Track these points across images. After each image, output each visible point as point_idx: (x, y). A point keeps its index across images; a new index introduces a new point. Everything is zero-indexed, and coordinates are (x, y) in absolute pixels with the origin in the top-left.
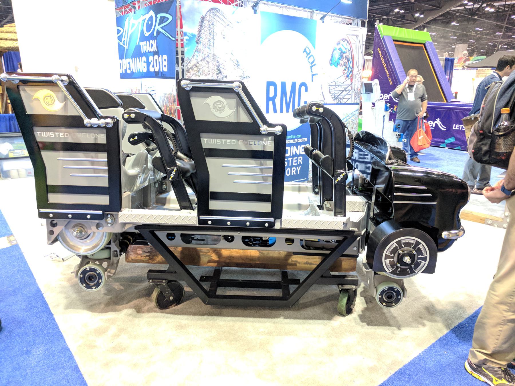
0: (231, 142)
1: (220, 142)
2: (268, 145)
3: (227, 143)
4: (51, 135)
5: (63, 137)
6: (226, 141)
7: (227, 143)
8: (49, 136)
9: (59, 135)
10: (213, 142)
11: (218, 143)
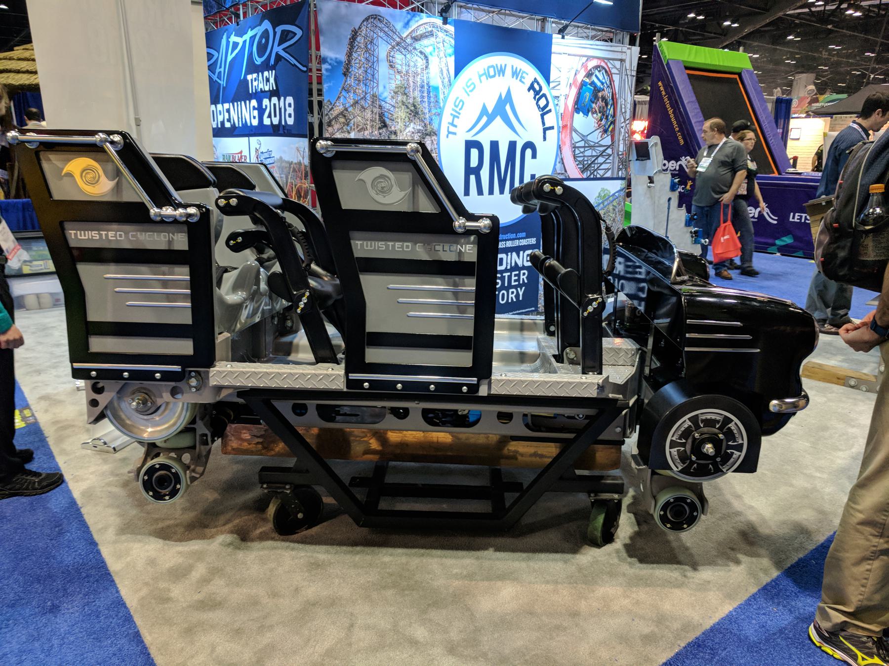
0: (402, 247)
1: (384, 246)
3: (397, 249)
4: (93, 235)
5: (401, 249)
6: (395, 245)
7: (397, 249)
8: (377, 248)
9: (107, 235)
10: (371, 247)
11: (380, 249)
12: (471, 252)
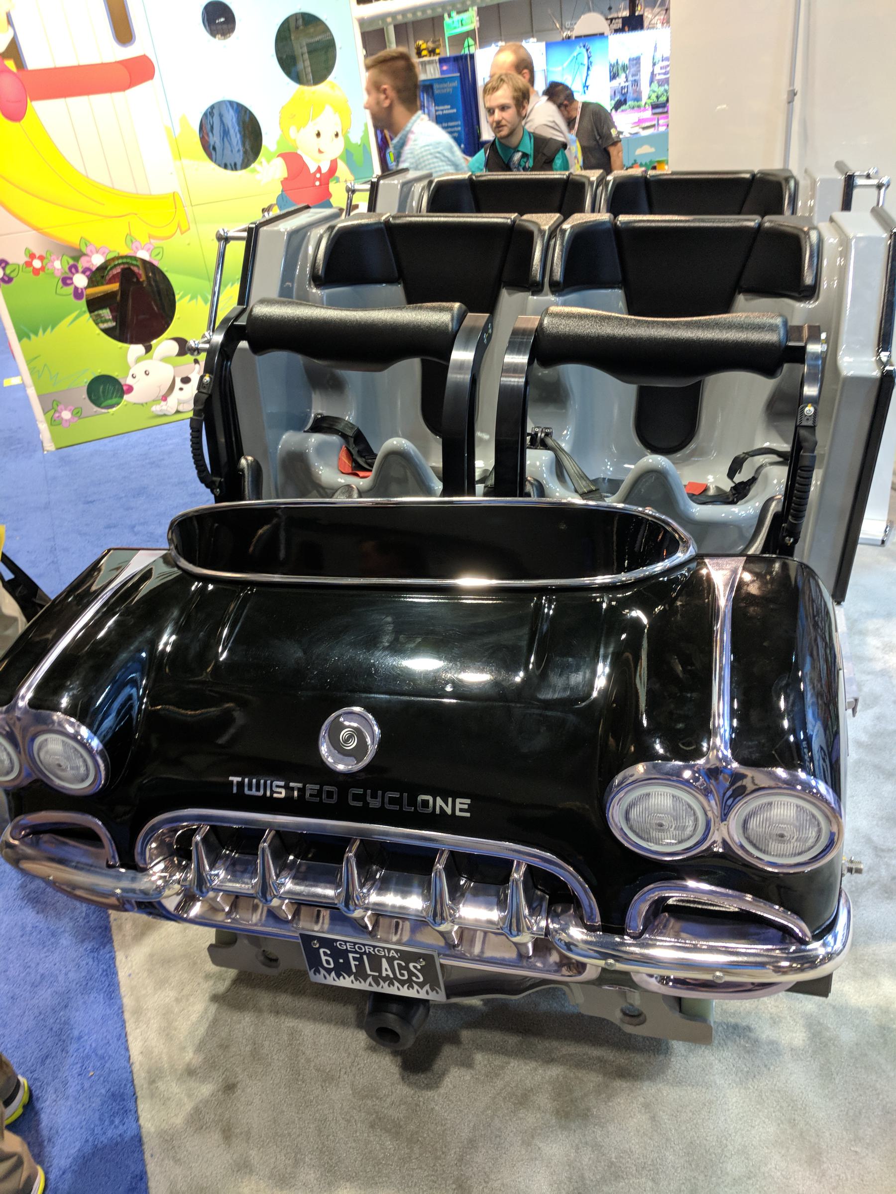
1: (283, 791)
2: (458, 813)
9: (302, 791)
11: (275, 795)
12: (468, 815)
